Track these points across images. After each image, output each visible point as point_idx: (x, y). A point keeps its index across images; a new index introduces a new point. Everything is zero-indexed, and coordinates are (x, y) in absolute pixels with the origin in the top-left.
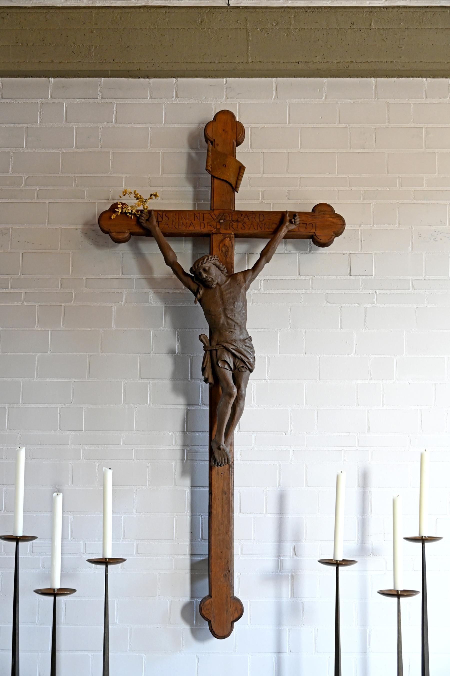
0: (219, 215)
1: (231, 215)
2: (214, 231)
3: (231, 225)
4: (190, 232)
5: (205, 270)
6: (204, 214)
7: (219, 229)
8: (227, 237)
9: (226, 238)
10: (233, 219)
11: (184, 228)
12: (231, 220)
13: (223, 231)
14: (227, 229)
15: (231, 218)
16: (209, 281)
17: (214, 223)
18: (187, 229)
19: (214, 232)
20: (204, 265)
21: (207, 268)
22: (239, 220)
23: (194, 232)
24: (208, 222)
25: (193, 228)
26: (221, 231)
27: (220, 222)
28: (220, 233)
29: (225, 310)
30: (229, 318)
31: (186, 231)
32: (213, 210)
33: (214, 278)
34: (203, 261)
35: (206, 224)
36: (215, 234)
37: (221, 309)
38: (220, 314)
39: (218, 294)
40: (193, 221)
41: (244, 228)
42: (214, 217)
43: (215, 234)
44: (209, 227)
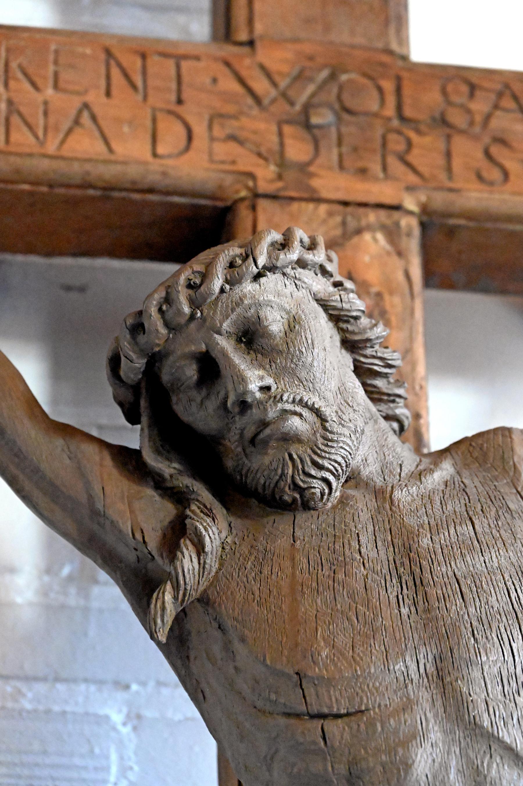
0: (300, 77)
1: (388, 86)
2: (266, 175)
3: (396, 144)
4: (76, 170)
5: (251, 337)
6: (179, 59)
7: (303, 168)
8: (369, 228)
9: (359, 231)
10: (408, 112)
11: (22, 137)
12: (390, 111)
13: (332, 183)
14: (363, 172)
15: (391, 100)
16: (289, 438)
17: (261, 127)
18: (51, 148)
19: (263, 187)
20: (248, 287)
21: (275, 323)
22: (457, 118)
23: (109, 172)
24: (215, 118)
25: (100, 147)
26: (316, 183)
27: (308, 126)
28: (318, 200)
29: (445, 680)
30: (491, 739)
31: (44, 165)
32: (251, 43)
33: (328, 412)
34: (249, 255)
35: (200, 129)
36: (273, 197)
37: (412, 665)
38: (408, 705)
39: (371, 549)
40: (96, 98)
41: (496, 175)
42: (261, 85)
43: (273, 197)
44: (222, 150)
